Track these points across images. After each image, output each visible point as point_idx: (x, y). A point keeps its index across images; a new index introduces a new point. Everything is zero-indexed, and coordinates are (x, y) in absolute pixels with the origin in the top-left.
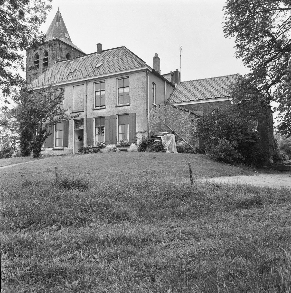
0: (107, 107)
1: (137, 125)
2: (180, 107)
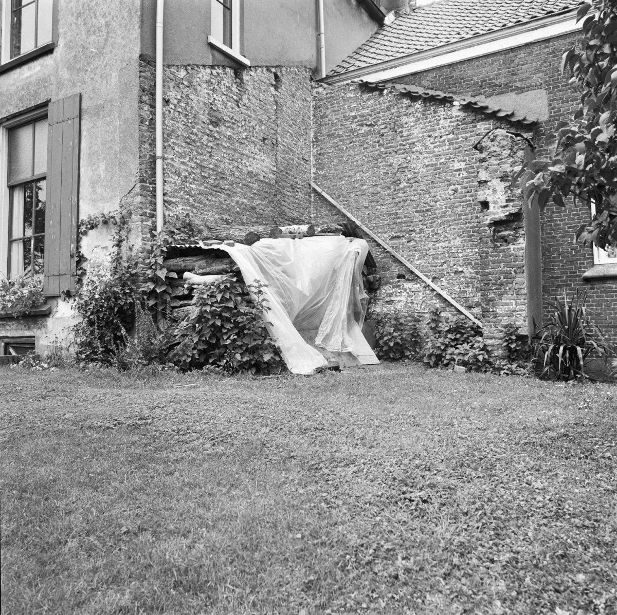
2: (398, 86)
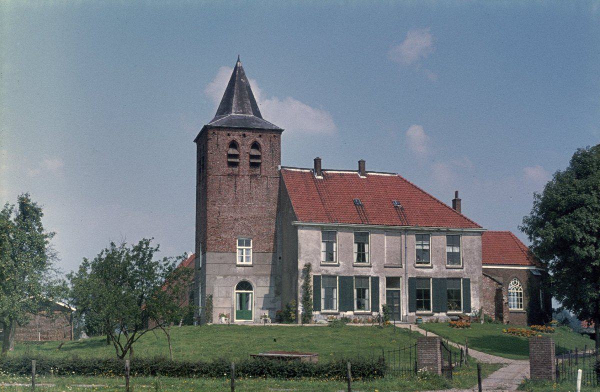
0: (435, 266)
1: (472, 292)
